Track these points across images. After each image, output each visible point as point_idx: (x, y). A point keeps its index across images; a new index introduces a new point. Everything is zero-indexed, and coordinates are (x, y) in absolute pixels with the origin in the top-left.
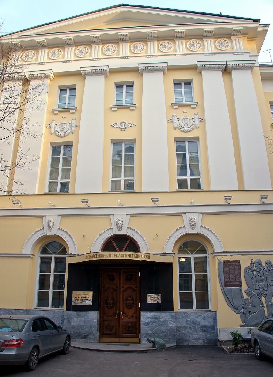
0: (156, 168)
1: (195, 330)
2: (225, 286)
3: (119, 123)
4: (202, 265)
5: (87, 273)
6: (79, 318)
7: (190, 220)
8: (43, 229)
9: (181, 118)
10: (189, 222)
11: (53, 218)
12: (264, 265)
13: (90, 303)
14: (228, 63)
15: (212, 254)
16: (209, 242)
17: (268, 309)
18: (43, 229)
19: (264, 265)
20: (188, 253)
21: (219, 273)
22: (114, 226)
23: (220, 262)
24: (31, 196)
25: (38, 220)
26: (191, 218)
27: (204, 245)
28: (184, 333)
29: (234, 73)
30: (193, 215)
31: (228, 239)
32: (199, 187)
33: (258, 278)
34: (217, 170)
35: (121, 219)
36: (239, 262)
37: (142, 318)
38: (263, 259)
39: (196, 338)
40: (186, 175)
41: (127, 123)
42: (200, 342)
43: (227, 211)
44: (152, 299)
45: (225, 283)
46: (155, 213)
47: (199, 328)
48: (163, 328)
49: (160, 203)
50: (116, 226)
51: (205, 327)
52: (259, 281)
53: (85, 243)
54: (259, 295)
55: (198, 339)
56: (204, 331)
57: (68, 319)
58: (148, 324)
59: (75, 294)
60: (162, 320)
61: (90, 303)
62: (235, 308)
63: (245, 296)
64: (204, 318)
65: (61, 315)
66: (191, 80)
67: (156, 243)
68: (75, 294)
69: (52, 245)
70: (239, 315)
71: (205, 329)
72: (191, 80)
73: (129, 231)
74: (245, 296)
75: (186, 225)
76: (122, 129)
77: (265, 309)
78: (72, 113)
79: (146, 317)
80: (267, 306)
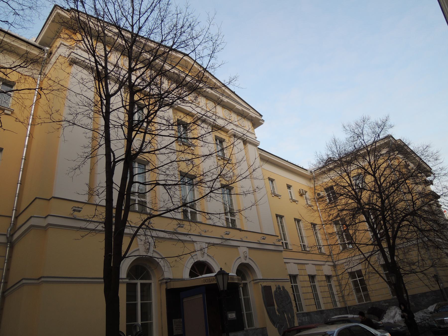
12: (282, 289)
19: (282, 289)
36: (270, 287)
38: (281, 284)
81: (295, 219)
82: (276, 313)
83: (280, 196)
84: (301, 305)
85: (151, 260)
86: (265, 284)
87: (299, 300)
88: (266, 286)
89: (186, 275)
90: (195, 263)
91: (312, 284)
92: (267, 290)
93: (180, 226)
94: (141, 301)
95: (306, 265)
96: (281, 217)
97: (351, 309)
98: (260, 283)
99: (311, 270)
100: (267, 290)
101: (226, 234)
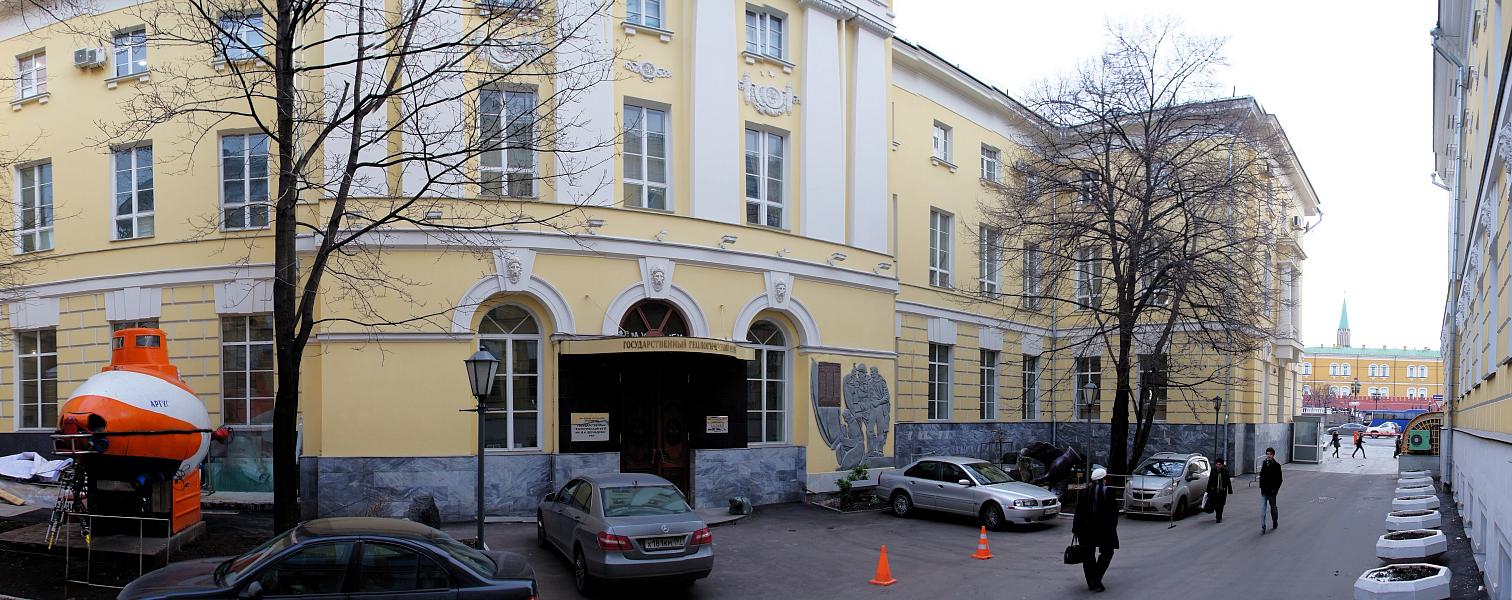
0: (711, 178)
1: (769, 479)
2: (820, 405)
3: (640, 64)
4: (527, 361)
5: (587, 379)
6: (586, 467)
7: (655, 272)
8: (766, 296)
9: (759, 85)
10: (774, 289)
11: (658, 262)
12: (869, 374)
13: (605, 437)
14: (860, 12)
15: (798, 348)
16: (548, 316)
17: (868, 443)
18: (766, 296)
19: (869, 374)
20: (499, 332)
21: (812, 383)
22: (646, 280)
23: (814, 363)
24: (696, 222)
25: (630, 266)
26: (778, 282)
27: (534, 316)
28: (756, 485)
29: (862, 33)
30: (780, 276)
31: (838, 328)
32: (662, 206)
33: (861, 394)
34: (816, 202)
35: (661, 268)
36: (838, 366)
37: (697, 462)
38: (869, 364)
39: (771, 491)
40: (640, 177)
41: (657, 68)
42: (775, 499)
43: (828, 278)
44: (717, 424)
45: (820, 399)
46: (719, 263)
47: (774, 475)
48: (731, 479)
49: (598, 232)
50: (651, 281)
51: (782, 472)
52: (861, 399)
53: (589, 312)
54: (859, 421)
55: (772, 493)
56: (781, 479)
57: (565, 470)
58: (707, 471)
59: (577, 418)
60: (730, 464)
61: (605, 437)
62: (830, 440)
63: (843, 422)
64: (782, 458)
65: (539, 463)
66: (786, 15)
67: (719, 324)
68: (577, 418)
69: (510, 314)
70: (834, 452)
71: (783, 475)
72: (786, 15)
73: (793, 305)
74: (843, 422)
75: (768, 293)
76: (645, 78)
77: (865, 443)
78: (663, 42)
79: (704, 458)
80: (868, 438)
81: (934, 212)
82: (1127, 414)
83: (955, 167)
84: (991, 407)
85: (785, 314)
86: (826, 358)
87: (991, 398)
88: (826, 364)
89: (613, 328)
90: (645, 300)
91: (1027, 372)
92: (827, 373)
93: (885, 267)
94: (760, 382)
95: (930, 320)
96: (946, 217)
97: (1061, 428)
98: (810, 356)
99: (992, 340)
100: (827, 373)
101: (836, 258)
